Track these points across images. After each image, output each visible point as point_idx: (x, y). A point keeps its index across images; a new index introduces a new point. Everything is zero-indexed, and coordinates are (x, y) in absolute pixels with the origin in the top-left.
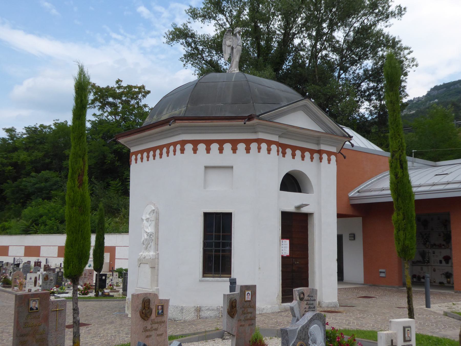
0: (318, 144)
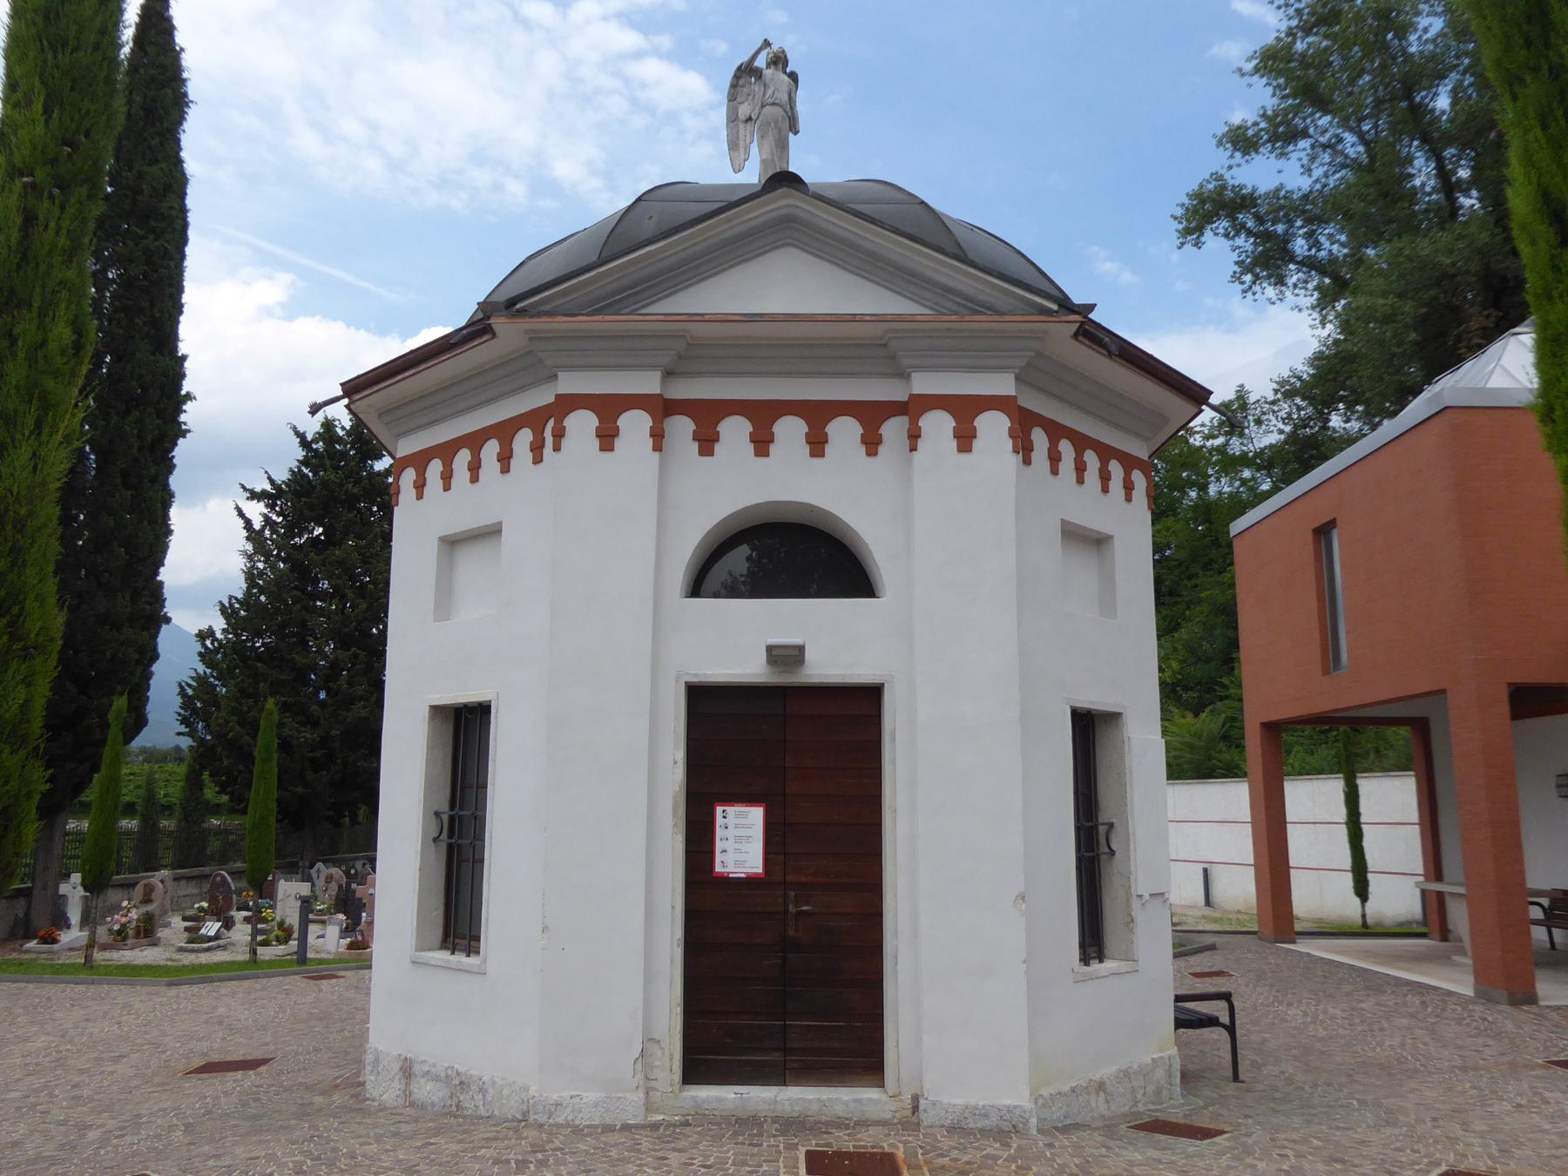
0: (904, 376)
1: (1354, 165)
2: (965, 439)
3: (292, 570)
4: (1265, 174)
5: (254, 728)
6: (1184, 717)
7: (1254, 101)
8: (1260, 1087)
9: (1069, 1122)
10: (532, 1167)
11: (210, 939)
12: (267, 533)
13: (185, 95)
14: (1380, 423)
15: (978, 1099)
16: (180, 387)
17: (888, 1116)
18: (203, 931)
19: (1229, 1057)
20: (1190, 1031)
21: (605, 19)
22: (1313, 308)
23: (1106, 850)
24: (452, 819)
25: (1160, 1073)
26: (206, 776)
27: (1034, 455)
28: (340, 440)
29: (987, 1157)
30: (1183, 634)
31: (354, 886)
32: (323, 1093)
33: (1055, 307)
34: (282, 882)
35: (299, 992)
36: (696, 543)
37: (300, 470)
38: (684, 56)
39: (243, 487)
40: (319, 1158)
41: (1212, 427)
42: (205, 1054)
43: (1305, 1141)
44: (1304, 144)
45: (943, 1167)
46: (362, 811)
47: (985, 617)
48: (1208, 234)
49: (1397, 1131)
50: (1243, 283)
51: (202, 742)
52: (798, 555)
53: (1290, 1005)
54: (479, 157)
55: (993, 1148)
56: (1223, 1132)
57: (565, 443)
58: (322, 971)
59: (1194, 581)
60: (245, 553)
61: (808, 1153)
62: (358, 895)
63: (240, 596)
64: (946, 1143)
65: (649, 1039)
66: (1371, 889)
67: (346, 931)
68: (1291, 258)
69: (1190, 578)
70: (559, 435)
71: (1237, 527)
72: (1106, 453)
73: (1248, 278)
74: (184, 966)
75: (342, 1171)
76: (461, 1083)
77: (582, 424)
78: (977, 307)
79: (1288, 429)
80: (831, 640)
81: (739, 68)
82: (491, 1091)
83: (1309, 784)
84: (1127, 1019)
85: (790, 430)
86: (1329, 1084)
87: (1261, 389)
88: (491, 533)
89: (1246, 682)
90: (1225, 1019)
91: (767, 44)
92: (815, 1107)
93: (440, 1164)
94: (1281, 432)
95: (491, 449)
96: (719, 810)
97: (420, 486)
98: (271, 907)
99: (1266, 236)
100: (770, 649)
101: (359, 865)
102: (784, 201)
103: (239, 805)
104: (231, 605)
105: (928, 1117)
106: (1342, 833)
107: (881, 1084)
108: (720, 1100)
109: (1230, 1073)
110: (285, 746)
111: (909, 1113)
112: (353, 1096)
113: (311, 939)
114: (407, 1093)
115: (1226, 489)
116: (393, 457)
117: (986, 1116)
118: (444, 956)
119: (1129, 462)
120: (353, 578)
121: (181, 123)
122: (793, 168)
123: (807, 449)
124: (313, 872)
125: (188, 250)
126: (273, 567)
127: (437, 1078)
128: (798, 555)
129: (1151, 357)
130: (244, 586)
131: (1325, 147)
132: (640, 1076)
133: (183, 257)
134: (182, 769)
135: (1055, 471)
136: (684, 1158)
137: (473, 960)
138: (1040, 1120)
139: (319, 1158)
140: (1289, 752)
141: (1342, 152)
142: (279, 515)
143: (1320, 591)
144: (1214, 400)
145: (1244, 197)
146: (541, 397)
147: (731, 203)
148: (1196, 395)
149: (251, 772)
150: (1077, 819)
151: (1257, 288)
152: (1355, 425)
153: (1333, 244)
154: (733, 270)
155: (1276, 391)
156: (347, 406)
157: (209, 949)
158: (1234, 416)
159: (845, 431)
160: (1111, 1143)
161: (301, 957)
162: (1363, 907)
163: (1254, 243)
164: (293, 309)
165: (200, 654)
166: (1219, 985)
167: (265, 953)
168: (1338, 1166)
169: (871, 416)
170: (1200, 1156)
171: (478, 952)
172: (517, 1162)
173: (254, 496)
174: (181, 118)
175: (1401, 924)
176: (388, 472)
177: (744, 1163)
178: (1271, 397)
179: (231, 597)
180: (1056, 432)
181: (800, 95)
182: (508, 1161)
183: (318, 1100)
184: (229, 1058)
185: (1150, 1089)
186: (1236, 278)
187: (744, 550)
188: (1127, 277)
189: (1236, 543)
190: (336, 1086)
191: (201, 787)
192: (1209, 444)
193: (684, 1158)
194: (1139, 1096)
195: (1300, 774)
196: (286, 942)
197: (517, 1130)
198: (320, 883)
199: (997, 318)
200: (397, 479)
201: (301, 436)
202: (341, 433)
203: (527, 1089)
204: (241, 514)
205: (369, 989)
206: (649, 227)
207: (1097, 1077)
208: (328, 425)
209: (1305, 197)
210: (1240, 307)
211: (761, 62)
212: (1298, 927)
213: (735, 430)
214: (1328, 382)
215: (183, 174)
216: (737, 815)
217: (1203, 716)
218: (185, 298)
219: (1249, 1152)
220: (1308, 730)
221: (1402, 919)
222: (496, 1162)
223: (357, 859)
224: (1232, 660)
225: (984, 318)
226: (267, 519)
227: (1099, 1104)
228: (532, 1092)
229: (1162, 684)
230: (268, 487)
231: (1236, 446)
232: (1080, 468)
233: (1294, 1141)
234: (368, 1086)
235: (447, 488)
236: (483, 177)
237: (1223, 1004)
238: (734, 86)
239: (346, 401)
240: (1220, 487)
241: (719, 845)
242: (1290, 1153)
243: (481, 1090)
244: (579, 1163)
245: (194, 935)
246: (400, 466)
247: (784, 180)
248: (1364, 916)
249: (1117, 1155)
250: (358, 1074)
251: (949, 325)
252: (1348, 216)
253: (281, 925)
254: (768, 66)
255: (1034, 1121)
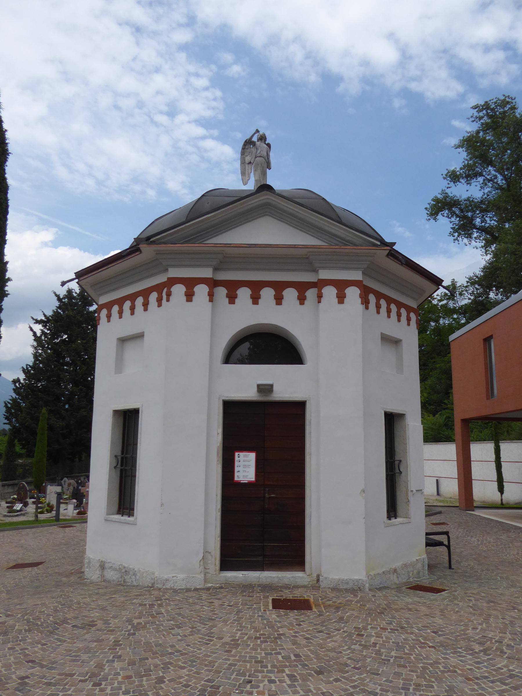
0: (315, 271)
1: (500, 188)
2: (341, 298)
3: (54, 353)
4: (463, 191)
5: (37, 420)
6: (429, 416)
7: (459, 160)
8: (460, 571)
9: (381, 586)
10: (156, 607)
11: (18, 511)
12: (43, 338)
13: (7, 150)
14: (510, 296)
15: (344, 576)
16: (5, 275)
17: (306, 583)
18: (15, 508)
19: (447, 558)
20: (431, 548)
21: (189, 122)
22: (482, 247)
23: (398, 471)
24: (122, 458)
25: (419, 565)
26: (16, 441)
27: (370, 305)
28: (74, 298)
29: (348, 601)
30: (429, 382)
31: (80, 487)
32: (67, 576)
33: (379, 243)
34: (49, 486)
35: (57, 534)
36: (228, 340)
37: (57, 311)
38: (223, 139)
39: (32, 318)
40: (64, 604)
41: (441, 296)
42: (15, 560)
43: (478, 594)
44: (481, 179)
45: (329, 605)
46: (84, 456)
47: (349, 374)
48: (440, 216)
49: (516, 590)
50: (454, 236)
51: (14, 427)
52: (271, 346)
53: (472, 537)
54: (136, 180)
55: (350, 597)
56: (444, 590)
57: (171, 298)
58: (66, 524)
59: (434, 360)
60: (33, 346)
61: (273, 600)
62: (82, 491)
63: (31, 364)
64: (331, 595)
65: (206, 552)
66: (505, 489)
67: (76, 507)
68: (475, 227)
69: (432, 359)
70: (169, 295)
71: (452, 337)
72: (400, 305)
73: (456, 234)
74: (6, 523)
75: (74, 610)
76: (125, 571)
77: (179, 290)
78: (346, 242)
79: (472, 298)
80: (284, 382)
81: (246, 141)
82: (138, 574)
83: (480, 444)
84: (406, 543)
85: (268, 293)
86: (488, 570)
87: (461, 281)
88: (140, 336)
89: (455, 402)
90: (446, 543)
91: (257, 131)
92: (276, 580)
93: (116, 606)
94: (469, 299)
95: (140, 301)
96: (237, 454)
97: (109, 316)
98: (44, 497)
99: (465, 217)
100: (258, 386)
101: (82, 479)
102: (265, 197)
103: (30, 454)
104: (27, 368)
105: (323, 584)
106: (493, 465)
107: (304, 570)
108: (236, 577)
109: (447, 565)
110: (51, 428)
111: (315, 582)
112: (79, 578)
113: (62, 510)
114: (102, 576)
115: (447, 322)
116: (97, 304)
117: (347, 583)
118: (118, 517)
119: (409, 310)
120: (80, 356)
121: (5, 163)
122: (269, 182)
123: (274, 302)
124: (63, 482)
125: (8, 217)
126: (45, 352)
127: (115, 570)
128: (271, 346)
129: (418, 265)
130: (33, 360)
131: (489, 181)
132: (202, 567)
133: (6, 220)
134: (6, 439)
135: (378, 312)
136: (220, 602)
137: (131, 519)
138: (370, 585)
139: (64, 604)
140: (472, 432)
141: (496, 183)
142: (48, 330)
143: (486, 364)
144: (444, 284)
145: (455, 201)
146: (161, 279)
147: (241, 197)
148: (437, 282)
149: (36, 439)
150: (386, 458)
151: (460, 239)
152: (500, 297)
153: (491, 221)
154: (244, 226)
155: (468, 282)
156: (77, 283)
157: (17, 516)
158: (453, 289)
159: (290, 294)
160: (399, 595)
161: (57, 518)
162: (501, 496)
163: (460, 221)
164: (55, 244)
165: (14, 389)
166: (443, 528)
167: (41, 517)
168: (492, 604)
169: (302, 288)
170: (436, 600)
171: (133, 515)
172: (150, 605)
173: (37, 322)
174: (5, 160)
175: (516, 504)
176: (95, 312)
177: (246, 604)
178: (465, 285)
179: (27, 365)
180: (379, 296)
181: (272, 154)
182: (145, 605)
183: (64, 579)
184: (27, 562)
185: (415, 572)
186: (451, 234)
187: (247, 345)
188: (407, 234)
189: (452, 346)
190: (72, 573)
191: (14, 446)
192: (440, 304)
193: (220, 602)
194: (411, 575)
195: (476, 441)
196: (51, 512)
197: (149, 591)
198: (66, 486)
199: (355, 247)
200: (99, 314)
201: (58, 296)
202: (75, 295)
203: (153, 573)
204: (31, 330)
205: (86, 531)
206: (207, 207)
207: (394, 567)
208: (70, 291)
209: (482, 202)
210: (453, 247)
211: (255, 139)
212: (475, 504)
213: (244, 293)
214: (489, 278)
215: (6, 184)
216: (244, 456)
217: (437, 416)
218: (7, 237)
219: (455, 598)
220: (480, 422)
221: (517, 501)
222: (141, 605)
223: (82, 476)
224: (449, 393)
225: (349, 247)
226: (43, 332)
227: (394, 578)
228: (156, 574)
229: (422, 402)
230: (43, 318)
231: (451, 304)
232: (389, 311)
233: (473, 594)
234: (86, 573)
235: (121, 317)
236: (137, 188)
237: (445, 536)
238: (243, 149)
239: (77, 280)
240: (444, 322)
241: (236, 469)
242: (472, 599)
243: (134, 574)
244: (176, 605)
245: (11, 510)
246: (101, 307)
247: (265, 188)
248: (502, 500)
249: (401, 600)
250: (81, 568)
251: (334, 250)
252: (499, 208)
253: (48, 505)
254: (258, 141)
255: (367, 585)
